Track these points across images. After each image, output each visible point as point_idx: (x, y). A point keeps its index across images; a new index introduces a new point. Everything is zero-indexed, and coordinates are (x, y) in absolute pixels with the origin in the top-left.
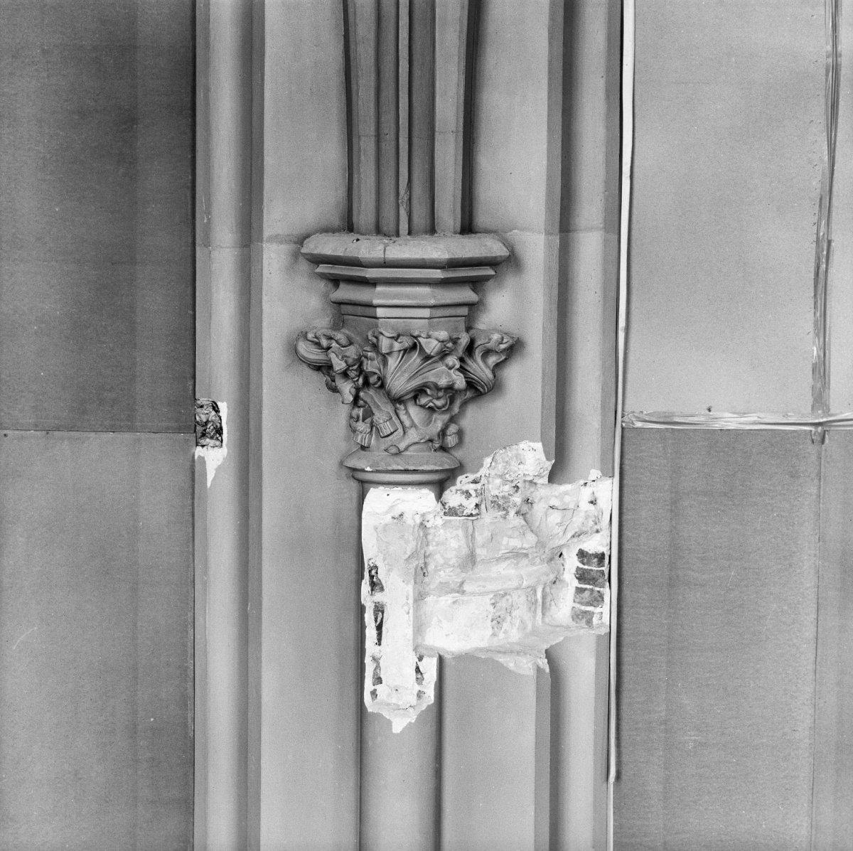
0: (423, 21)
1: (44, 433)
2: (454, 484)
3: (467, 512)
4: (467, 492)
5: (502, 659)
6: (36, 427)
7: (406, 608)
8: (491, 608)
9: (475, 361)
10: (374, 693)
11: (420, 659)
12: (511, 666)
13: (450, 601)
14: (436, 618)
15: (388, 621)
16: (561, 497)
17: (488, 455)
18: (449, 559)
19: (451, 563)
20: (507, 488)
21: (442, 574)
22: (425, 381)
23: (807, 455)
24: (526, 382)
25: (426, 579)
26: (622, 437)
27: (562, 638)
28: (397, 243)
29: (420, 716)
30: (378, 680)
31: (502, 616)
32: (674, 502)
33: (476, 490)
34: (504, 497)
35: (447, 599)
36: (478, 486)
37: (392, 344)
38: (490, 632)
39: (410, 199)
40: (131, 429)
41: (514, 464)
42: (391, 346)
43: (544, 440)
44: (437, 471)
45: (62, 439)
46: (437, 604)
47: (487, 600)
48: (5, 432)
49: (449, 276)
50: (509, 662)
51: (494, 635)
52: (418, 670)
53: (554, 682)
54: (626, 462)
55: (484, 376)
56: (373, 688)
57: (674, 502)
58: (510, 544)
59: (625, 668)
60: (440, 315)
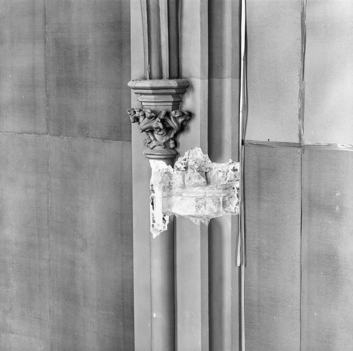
0: (304, 2)
1: (102, 140)
2: (177, 160)
3: (182, 170)
4: (182, 163)
5: (191, 219)
6: (101, 138)
7: (160, 199)
8: (195, 203)
9: (170, 119)
10: (153, 225)
11: (165, 216)
12: (194, 221)
13: (180, 199)
14: (175, 204)
15: (156, 203)
16: (222, 167)
17: (186, 151)
18: (178, 185)
19: (178, 186)
20: (193, 163)
21: (176, 189)
22: (151, 125)
23: (297, 158)
24: (197, 128)
25: (172, 191)
26: (244, 149)
27: (222, 215)
28: (141, 81)
29: (160, 234)
30: (154, 221)
31: (200, 205)
32: (259, 172)
33: (184, 163)
34: (192, 166)
35: (179, 198)
36: (186, 162)
37: (139, 114)
38: (195, 210)
39: (150, 68)
40: (121, 140)
41: (195, 154)
42: (139, 114)
43: (201, 147)
44: (161, 155)
45: (107, 142)
46: (176, 199)
47: (193, 200)
48: (94, 139)
49: (156, 92)
50: (193, 220)
51: (197, 211)
52: (164, 219)
53: (212, 228)
54: (245, 157)
55: (174, 126)
56: (153, 224)
57: (259, 172)
58: (195, 181)
59: (247, 228)
60: (160, 105)
